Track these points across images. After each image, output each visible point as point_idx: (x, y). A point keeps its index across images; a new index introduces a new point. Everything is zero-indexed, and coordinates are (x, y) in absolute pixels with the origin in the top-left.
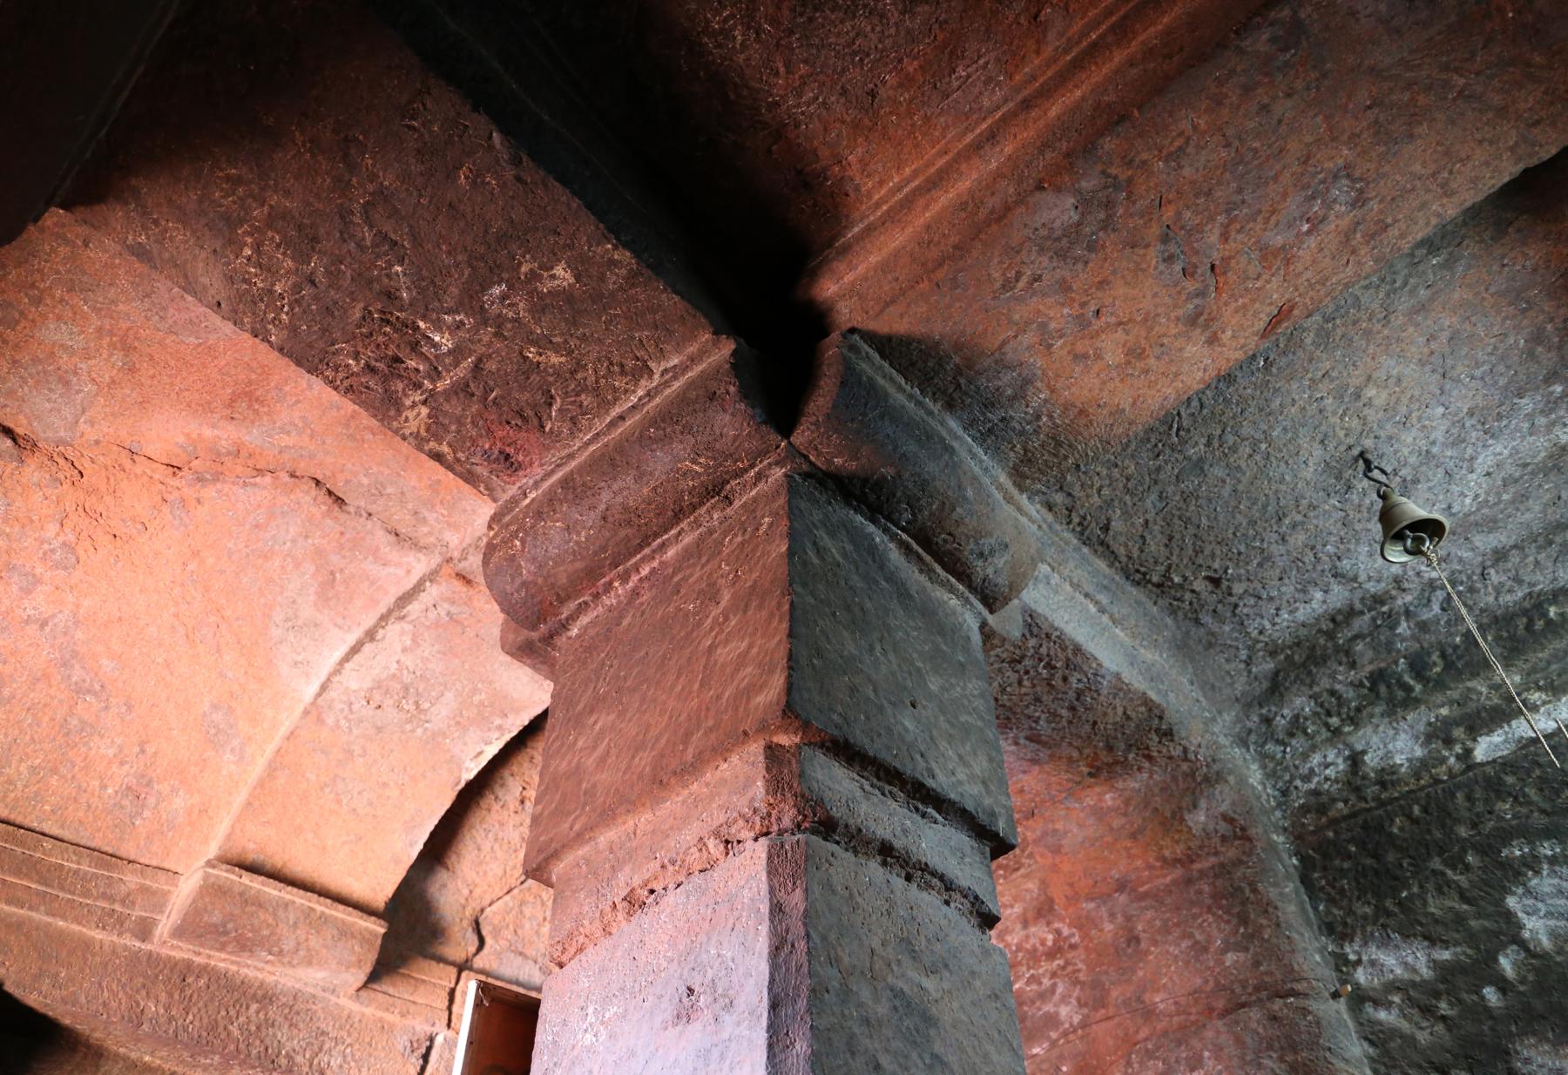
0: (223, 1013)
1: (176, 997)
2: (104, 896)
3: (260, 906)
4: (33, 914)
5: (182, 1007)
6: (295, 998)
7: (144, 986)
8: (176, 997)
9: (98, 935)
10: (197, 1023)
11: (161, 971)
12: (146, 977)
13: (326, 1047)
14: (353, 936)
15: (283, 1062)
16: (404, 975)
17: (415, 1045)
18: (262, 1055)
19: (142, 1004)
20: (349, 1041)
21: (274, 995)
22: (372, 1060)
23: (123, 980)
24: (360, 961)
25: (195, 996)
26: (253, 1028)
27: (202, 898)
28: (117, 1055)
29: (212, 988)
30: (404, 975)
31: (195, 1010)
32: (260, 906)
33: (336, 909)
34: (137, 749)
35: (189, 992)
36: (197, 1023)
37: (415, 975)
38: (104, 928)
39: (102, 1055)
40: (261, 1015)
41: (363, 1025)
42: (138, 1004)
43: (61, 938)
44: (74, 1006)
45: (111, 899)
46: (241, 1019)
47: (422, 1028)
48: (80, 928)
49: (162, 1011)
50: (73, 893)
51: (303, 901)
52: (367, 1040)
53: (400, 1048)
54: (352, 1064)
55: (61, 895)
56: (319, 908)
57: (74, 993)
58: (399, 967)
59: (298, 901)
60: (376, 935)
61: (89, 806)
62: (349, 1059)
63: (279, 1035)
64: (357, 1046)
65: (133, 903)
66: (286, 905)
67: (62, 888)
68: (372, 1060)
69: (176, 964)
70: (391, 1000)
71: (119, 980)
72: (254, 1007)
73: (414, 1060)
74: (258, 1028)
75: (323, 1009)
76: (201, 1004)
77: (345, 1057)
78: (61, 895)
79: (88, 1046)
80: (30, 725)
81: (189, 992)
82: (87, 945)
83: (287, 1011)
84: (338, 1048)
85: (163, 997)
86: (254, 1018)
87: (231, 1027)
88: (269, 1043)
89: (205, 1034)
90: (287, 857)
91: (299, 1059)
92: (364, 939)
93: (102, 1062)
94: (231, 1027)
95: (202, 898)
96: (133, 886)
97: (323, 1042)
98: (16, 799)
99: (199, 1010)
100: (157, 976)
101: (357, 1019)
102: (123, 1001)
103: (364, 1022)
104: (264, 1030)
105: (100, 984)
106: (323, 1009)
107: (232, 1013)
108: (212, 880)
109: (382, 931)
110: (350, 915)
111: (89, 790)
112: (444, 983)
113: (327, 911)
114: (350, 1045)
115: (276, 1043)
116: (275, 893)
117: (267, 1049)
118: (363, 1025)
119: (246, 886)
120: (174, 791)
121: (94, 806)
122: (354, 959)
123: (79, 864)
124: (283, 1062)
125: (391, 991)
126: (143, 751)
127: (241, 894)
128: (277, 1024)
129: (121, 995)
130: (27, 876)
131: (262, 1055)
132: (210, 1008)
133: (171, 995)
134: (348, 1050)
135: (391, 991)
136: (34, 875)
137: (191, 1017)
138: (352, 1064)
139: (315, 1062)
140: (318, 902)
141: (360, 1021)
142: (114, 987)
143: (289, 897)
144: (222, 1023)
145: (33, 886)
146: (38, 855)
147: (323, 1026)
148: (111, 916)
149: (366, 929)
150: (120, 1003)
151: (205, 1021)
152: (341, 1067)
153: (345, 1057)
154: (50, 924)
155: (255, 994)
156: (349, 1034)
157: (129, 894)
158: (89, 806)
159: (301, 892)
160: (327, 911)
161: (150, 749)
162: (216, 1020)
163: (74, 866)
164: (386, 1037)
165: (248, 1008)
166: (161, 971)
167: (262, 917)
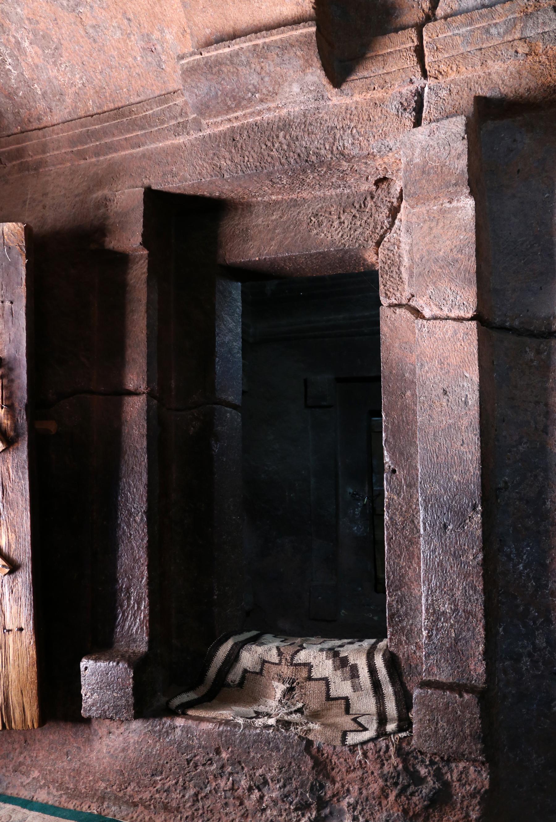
0: (264, 147)
1: (233, 151)
2: (171, 118)
3: (220, 64)
4: (146, 147)
5: (239, 155)
6: (305, 116)
7: (214, 154)
8: (233, 151)
9: (181, 140)
10: (251, 160)
11: (220, 142)
12: (213, 148)
13: (338, 136)
14: (292, 46)
15: (314, 158)
16: (372, 58)
17: (405, 104)
18: (298, 160)
19: (218, 164)
20: (352, 125)
21: (290, 121)
22: (375, 130)
23: (203, 157)
24: (307, 61)
25: (244, 146)
26: (285, 147)
27: (186, 81)
28: (258, 202)
29: (251, 136)
30: (369, 58)
31: (247, 153)
32: (220, 64)
33: (271, 35)
34: (126, 21)
35: (239, 146)
36: (251, 160)
37: (380, 53)
38: (179, 135)
39: (251, 205)
40: (288, 137)
41: (360, 109)
42: (217, 166)
43: (165, 151)
44: (186, 182)
45: (175, 118)
46: (276, 145)
47: (407, 90)
48: (170, 142)
49: (229, 163)
50: (157, 126)
51: (247, 44)
52: (366, 118)
53: (394, 111)
54: (361, 138)
55: (153, 130)
56: (260, 42)
57: (183, 175)
58: (365, 54)
59: (245, 45)
60: (310, 35)
61: (139, 75)
62: (357, 136)
63: (304, 143)
64: (360, 126)
65: (186, 113)
66: (237, 54)
67: (151, 126)
68: (375, 130)
69: (225, 134)
70: (368, 81)
71: (201, 158)
72: (281, 134)
73: (407, 115)
74: (289, 145)
75: (326, 113)
76: (250, 149)
77: (353, 137)
78: (153, 130)
79: (242, 204)
80: (79, 50)
81: (239, 146)
82: (178, 148)
83: (303, 126)
84: (346, 133)
85: (227, 155)
86: (284, 141)
87: (272, 153)
88: (299, 151)
89: (258, 164)
90: (232, 23)
91: (323, 152)
92: (302, 42)
93: (252, 209)
94: (272, 153)
95: (186, 81)
96: (182, 104)
97: (335, 134)
98: (111, 95)
99: (249, 152)
100: (218, 146)
101: (353, 108)
102: (208, 168)
103: (359, 107)
104: (293, 145)
105: (193, 165)
106: (326, 113)
107: (269, 144)
108: (185, 66)
109: (314, 29)
110: (283, 32)
111: (131, 66)
112: (408, 46)
113: (267, 40)
114: (355, 127)
115: (303, 149)
116: (227, 50)
117: (299, 155)
118: (360, 109)
119: (207, 57)
120: (162, 31)
121: (140, 73)
122: (301, 62)
123: (152, 109)
124: (314, 158)
125: (366, 74)
126: (129, 20)
127: (206, 63)
128: (299, 137)
129: (205, 165)
130: (134, 130)
131: (298, 160)
132: (256, 149)
133: (231, 152)
134: (354, 131)
135: (366, 74)
136: (135, 127)
137: (246, 159)
138: (361, 138)
139: (335, 148)
140: (258, 38)
141: (356, 108)
142: (200, 162)
143: (237, 47)
144: (266, 153)
145: (139, 133)
146: (134, 117)
147: (330, 124)
148: (178, 126)
149: (301, 35)
150: (207, 169)
151: (255, 156)
152: (353, 144)
153: (353, 137)
154: (157, 148)
155: (278, 127)
156: (351, 120)
157: (182, 110)
158: (139, 75)
159: (243, 38)
160: (267, 40)
161: (131, 16)
162: (261, 153)
163: (151, 112)
164: (379, 109)
165: (278, 137)
166: (220, 142)
167: (226, 71)
